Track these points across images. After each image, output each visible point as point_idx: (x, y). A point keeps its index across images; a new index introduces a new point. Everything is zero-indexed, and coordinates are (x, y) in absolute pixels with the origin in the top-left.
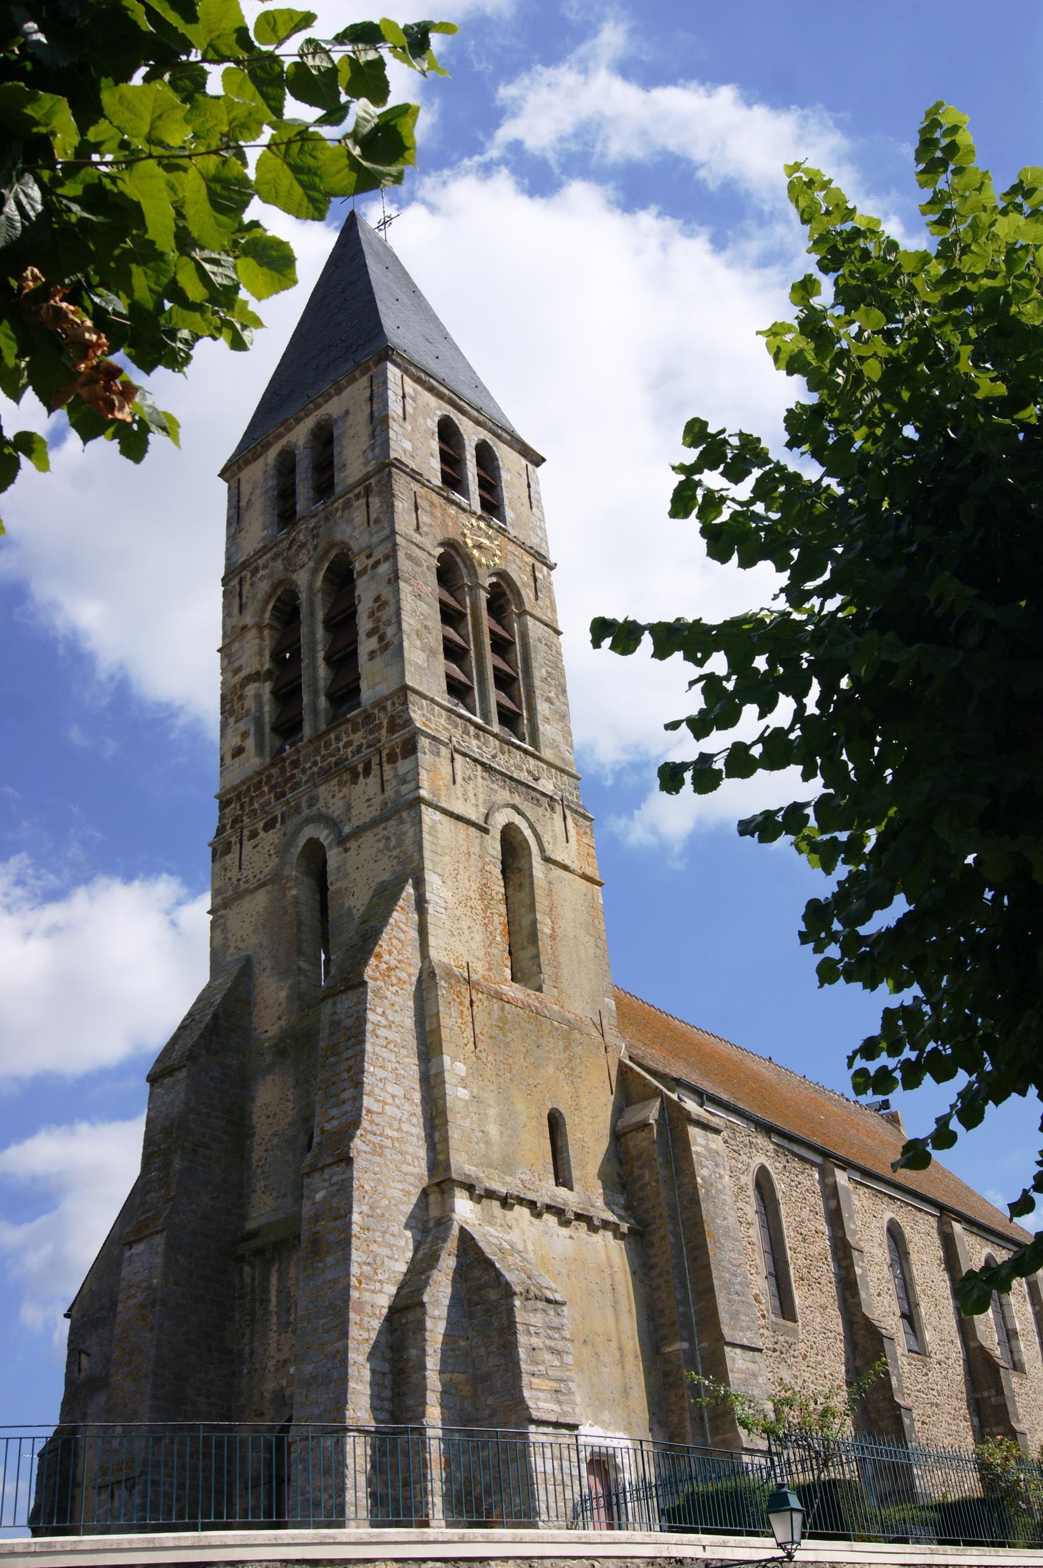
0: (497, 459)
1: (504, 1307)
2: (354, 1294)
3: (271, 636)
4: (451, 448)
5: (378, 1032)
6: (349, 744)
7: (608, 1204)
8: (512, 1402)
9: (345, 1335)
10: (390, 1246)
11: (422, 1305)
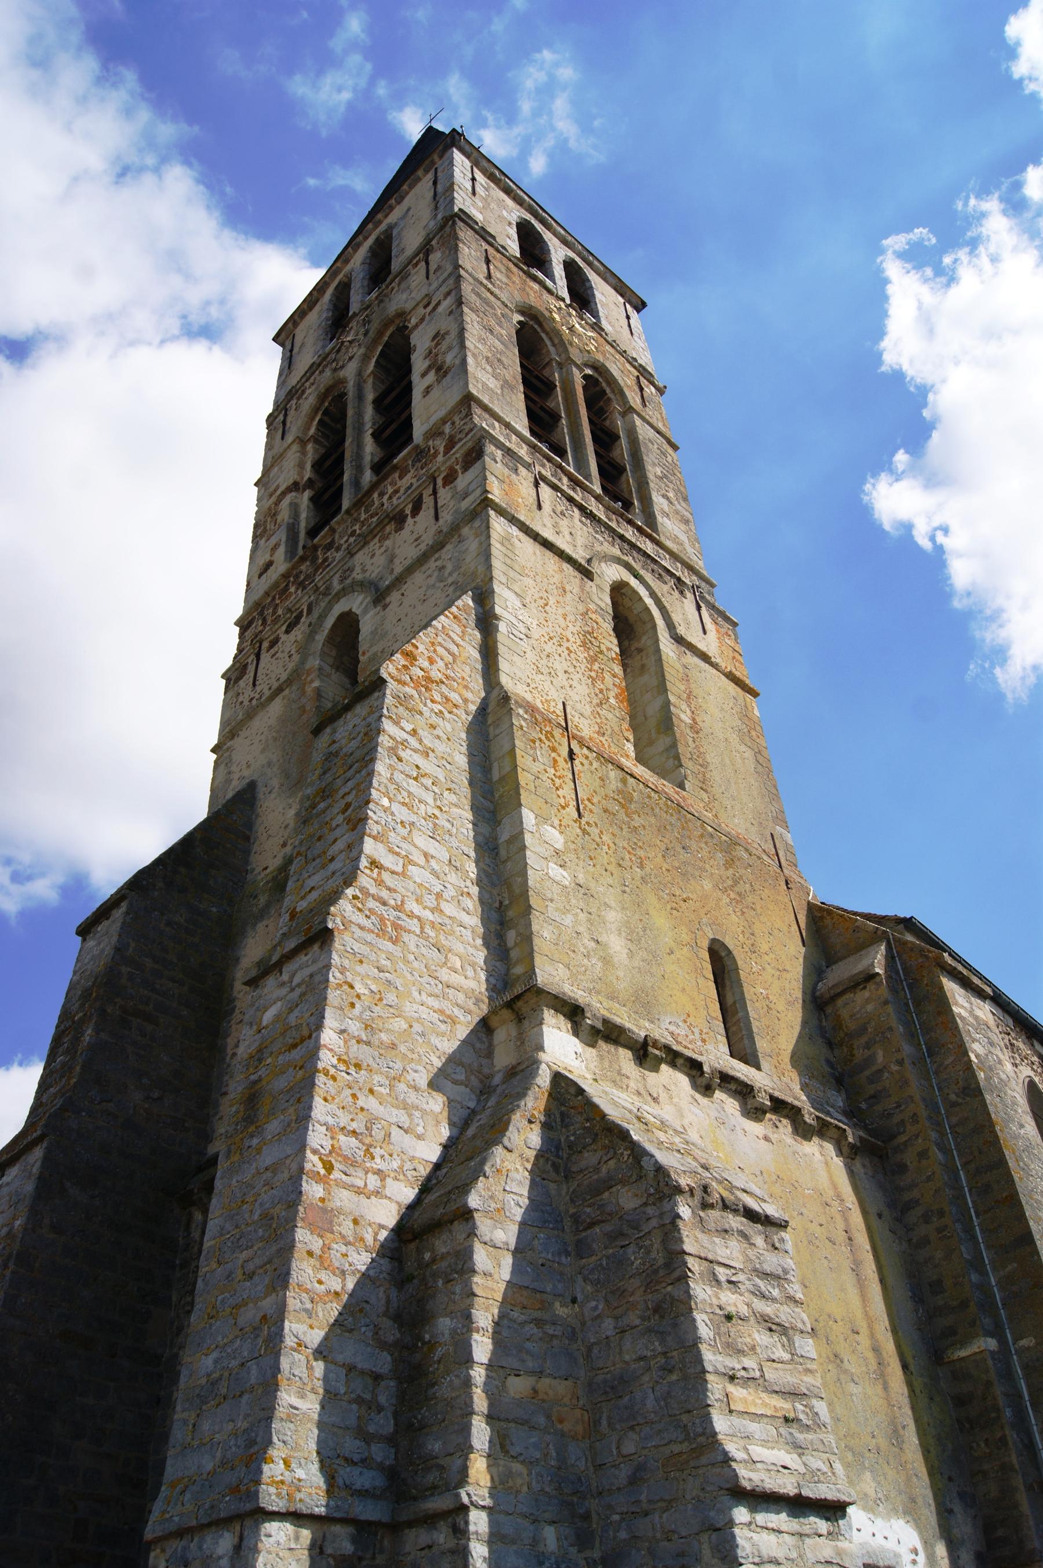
1: (654, 1223)
2: (312, 1190)
3: (316, 451)
5: (402, 754)
8: (685, 1447)
9: (281, 1279)
11: (467, 1215)
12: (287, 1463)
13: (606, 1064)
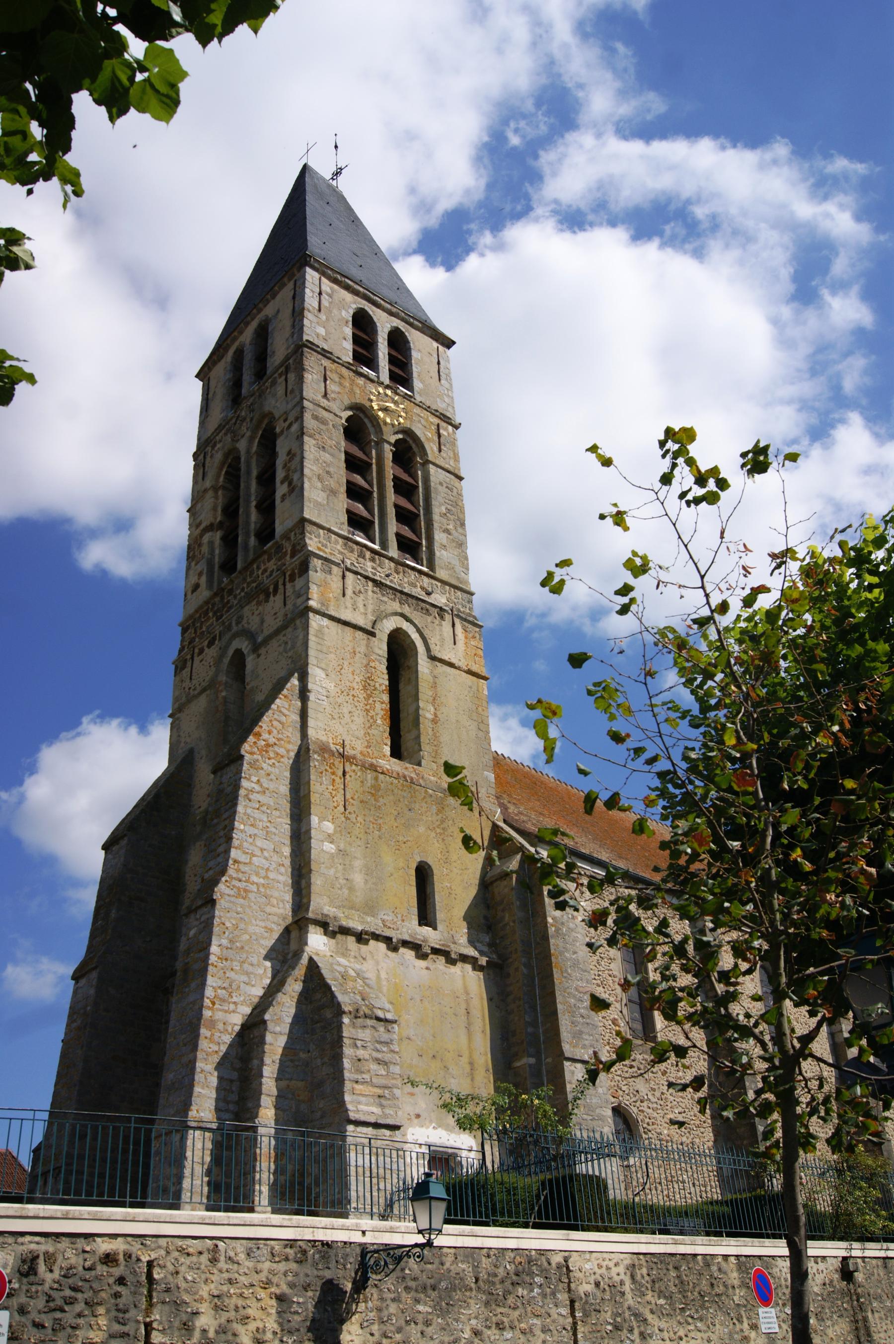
0: (408, 342)
1: (335, 1024)
2: (207, 1013)
4: (367, 334)
5: (251, 797)
6: (265, 570)
7: (472, 942)
9: (195, 1047)
10: (247, 974)
11: (264, 1022)
12: (197, 1111)
13: (340, 946)
